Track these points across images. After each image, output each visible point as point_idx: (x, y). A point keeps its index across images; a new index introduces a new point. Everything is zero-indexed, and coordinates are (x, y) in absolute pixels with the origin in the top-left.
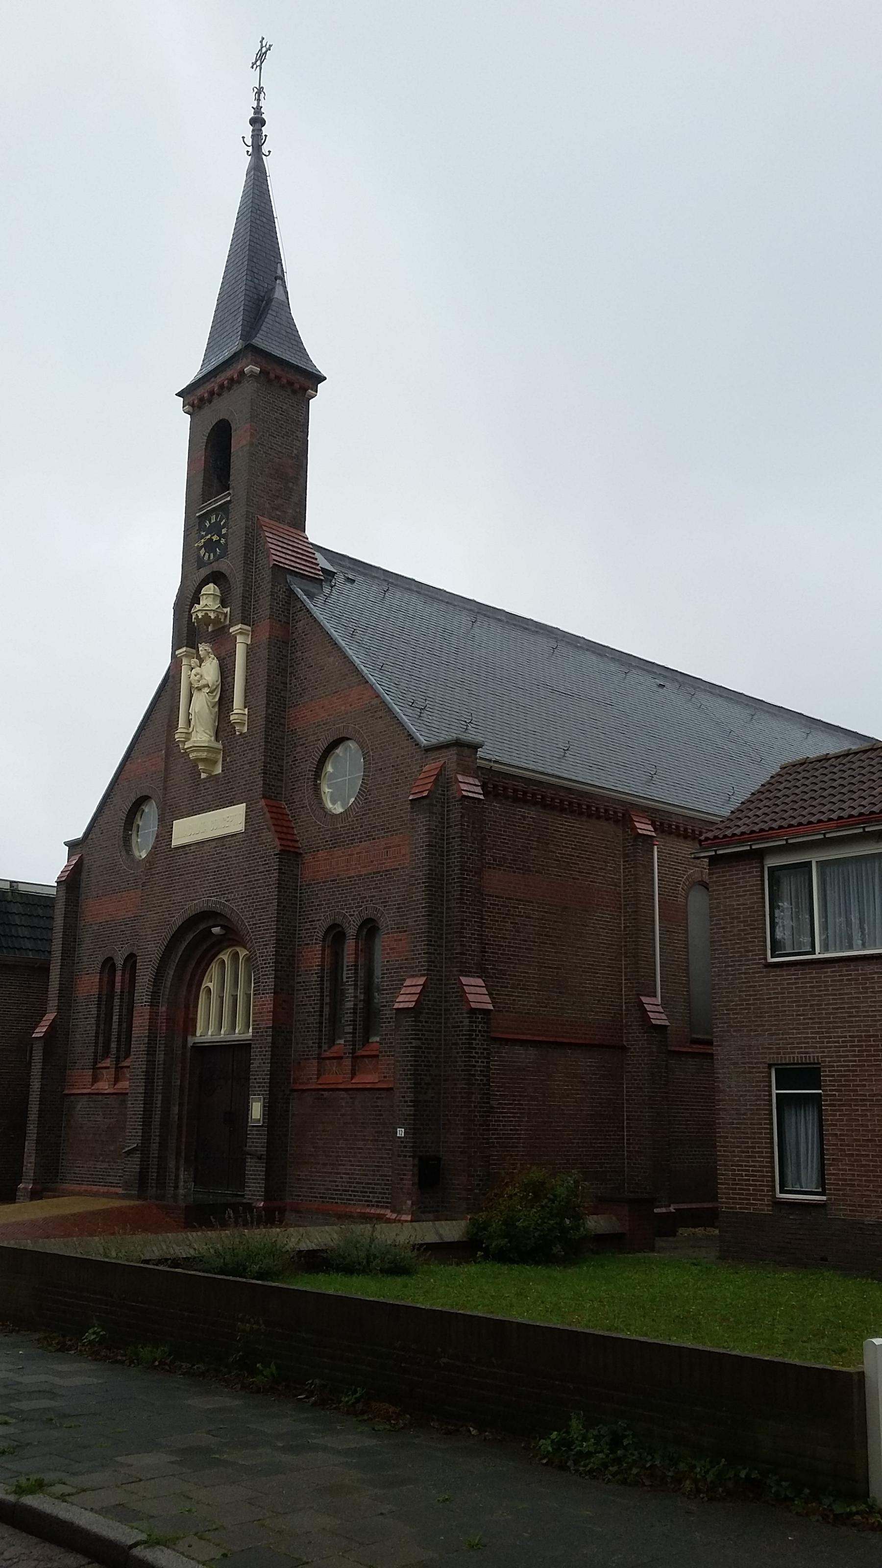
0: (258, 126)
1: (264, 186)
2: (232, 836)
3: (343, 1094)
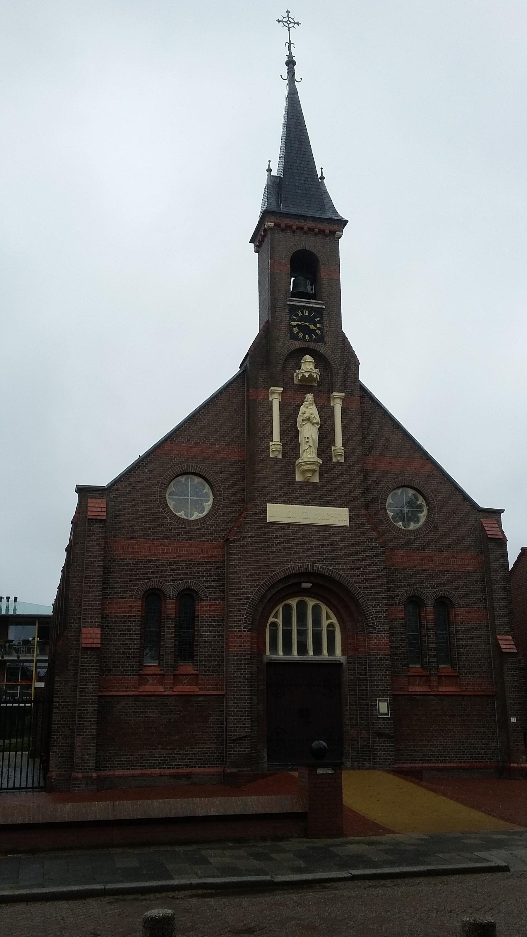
0: (291, 65)
1: (311, 157)
2: (335, 527)
3: (432, 698)
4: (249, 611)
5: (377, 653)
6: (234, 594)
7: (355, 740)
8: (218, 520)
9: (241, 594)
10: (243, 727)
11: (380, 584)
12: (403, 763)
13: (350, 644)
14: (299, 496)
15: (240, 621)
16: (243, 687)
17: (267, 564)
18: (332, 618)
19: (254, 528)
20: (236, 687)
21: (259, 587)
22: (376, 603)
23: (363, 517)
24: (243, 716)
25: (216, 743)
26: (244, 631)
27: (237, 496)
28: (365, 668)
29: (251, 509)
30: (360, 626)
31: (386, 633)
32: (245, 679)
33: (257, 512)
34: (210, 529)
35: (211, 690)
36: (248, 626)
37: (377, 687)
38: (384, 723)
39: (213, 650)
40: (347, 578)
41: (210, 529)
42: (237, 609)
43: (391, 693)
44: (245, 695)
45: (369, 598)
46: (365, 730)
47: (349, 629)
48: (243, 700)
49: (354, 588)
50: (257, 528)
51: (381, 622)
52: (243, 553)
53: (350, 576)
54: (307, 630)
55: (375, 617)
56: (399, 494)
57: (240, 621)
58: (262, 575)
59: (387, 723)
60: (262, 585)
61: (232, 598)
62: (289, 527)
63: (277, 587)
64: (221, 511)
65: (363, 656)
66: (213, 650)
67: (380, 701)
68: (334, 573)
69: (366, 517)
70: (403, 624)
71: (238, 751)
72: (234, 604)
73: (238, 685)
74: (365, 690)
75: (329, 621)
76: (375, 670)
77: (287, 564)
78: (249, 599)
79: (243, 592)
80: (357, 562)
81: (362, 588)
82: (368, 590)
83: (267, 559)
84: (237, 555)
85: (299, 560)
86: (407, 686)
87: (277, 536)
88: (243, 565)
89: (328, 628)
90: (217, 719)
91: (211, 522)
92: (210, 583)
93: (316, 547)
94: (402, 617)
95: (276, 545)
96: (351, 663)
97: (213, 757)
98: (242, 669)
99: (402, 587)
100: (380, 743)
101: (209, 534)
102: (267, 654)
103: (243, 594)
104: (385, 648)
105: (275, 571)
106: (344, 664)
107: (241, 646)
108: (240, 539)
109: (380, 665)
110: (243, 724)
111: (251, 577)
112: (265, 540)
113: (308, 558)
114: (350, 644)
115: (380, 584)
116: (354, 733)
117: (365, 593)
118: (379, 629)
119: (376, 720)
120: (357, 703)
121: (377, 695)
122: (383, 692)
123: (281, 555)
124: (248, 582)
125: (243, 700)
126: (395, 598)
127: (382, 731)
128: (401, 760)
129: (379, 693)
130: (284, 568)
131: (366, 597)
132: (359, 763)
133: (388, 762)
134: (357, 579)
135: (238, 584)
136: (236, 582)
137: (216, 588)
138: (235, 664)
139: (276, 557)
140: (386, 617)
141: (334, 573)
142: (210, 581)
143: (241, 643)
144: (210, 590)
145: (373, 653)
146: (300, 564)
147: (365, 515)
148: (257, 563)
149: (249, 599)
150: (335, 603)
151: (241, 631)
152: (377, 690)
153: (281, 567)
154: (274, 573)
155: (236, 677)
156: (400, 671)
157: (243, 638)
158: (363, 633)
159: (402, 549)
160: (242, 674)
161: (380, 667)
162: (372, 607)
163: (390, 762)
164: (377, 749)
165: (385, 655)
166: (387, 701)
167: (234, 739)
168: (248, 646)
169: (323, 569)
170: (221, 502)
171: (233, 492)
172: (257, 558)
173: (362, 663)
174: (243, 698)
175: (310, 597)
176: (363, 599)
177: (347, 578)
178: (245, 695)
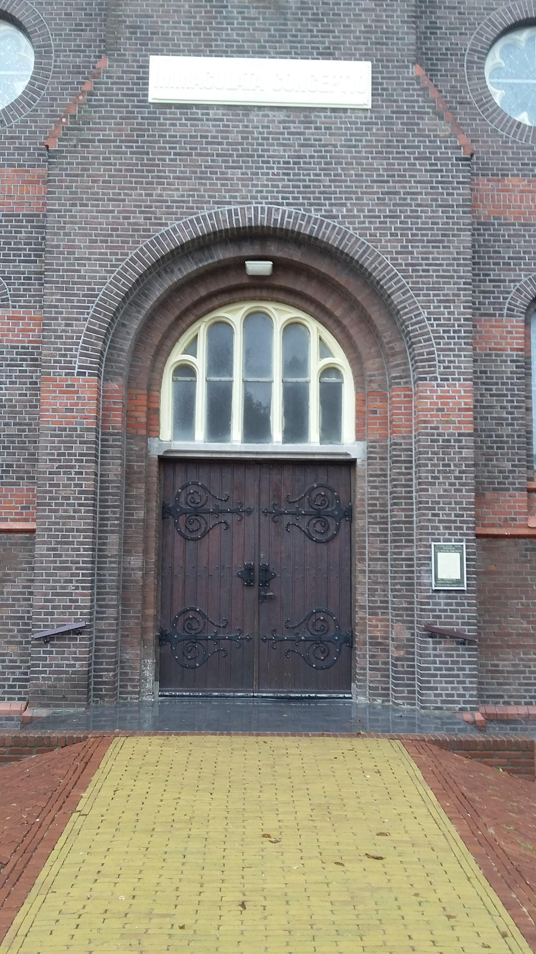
2: (334, 110)
4: (95, 325)
5: (437, 428)
6: (57, 283)
7: (380, 644)
8: (40, 116)
9: (74, 283)
10: (70, 607)
11: (451, 253)
12: (507, 703)
13: (375, 412)
14: (238, 35)
15: (71, 350)
16: (75, 511)
17: (146, 207)
18: (335, 354)
19: (115, 118)
20: (57, 511)
21: (123, 264)
22: (440, 301)
23: (412, 84)
24: (71, 581)
25: (21, 643)
26: (79, 374)
27: (90, 57)
28: (406, 468)
29: (108, 72)
30: (397, 366)
31: (465, 380)
32: (80, 492)
33: (122, 78)
34: (19, 138)
35: (12, 520)
36: (91, 362)
37: (434, 515)
38: (450, 604)
39: (20, 424)
40: (362, 239)
41: (19, 138)
42: (64, 319)
43: (473, 528)
44: (78, 530)
45: (421, 289)
46: (403, 622)
47: (370, 376)
48: (72, 543)
49: (380, 264)
50: (121, 118)
51: (453, 350)
52: (82, 181)
53: (371, 235)
54: (271, 382)
55: (435, 338)
56: (523, 45)
57: (71, 350)
58: (132, 236)
59: (457, 604)
60: (132, 259)
61: (52, 294)
62: (208, 114)
63: (180, 269)
64: (48, 94)
65: (404, 438)
66: (20, 424)
67: (439, 549)
68: (327, 228)
69: (418, 83)
70: (518, 361)
71: (57, 666)
72: (56, 307)
73: (62, 504)
74: (404, 522)
75: (327, 361)
76: (428, 471)
77: (197, 208)
78: (96, 296)
79: (79, 277)
80: (390, 200)
81: (401, 265)
82: (418, 271)
83: (146, 195)
84: (67, 187)
85: (231, 197)
86: (525, 514)
87: (175, 136)
88: (81, 211)
89: (326, 379)
90: (24, 587)
91: (22, 121)
92: (14, 267)
93: (279, 163)
94: (517, 344)
95: (171, 160)
96: (375, 458)
97: (12, 677)
98: (73, 467)
99: (520, 270)
100: (435, 656)
101: (16, 149)
102: (162, 437)
103: (80, 283)
104: (459, 416)
105: (166, 225)
106: (359, 462)
107: (72, 411)
108: (75, 146)
109: (444, 459)
110: (71, 601)
111: (102, 241)
112: (143, 147)
113: (257, 192)
114: (375, 412)
115: (451, 253)
116: (377, 626)
117: (411, 277)
118: (445, 368)
119: (429, 597)
120: (386, 553)
121: (434, 534)
122: (449, 528)
123: (185, 184)
124: (95, 253)
125: (72, 543)
126: (499, 298)
127: (441, 623)
128: (502, 697)
129: (437, 528)
130: (190, 217)
131: (412, 289)
132: (388, 701)
133: (458, 702)
134: (390, 241)
135: (69, 259)
136: (62, 253)
137: (30, 279)
138: (53, 454)
139: (171, 190)
140: (464, 338)
141: (327, 228)
142: (14, 261)
143: (71, 405)
144: (14, 284)
145: (426, 428)
146: (233, 207)
147: (418, 77)
148: (119, 206)
149: (96, 296)
150: (338, 313)
151: (73, 374)
152: (434, 521)
153: (182, 213)
154: (163, 229)
155: (58, 485)
156: (507, 478)
157: (77, 392)
158: (406, 383)
159: (524, 175)
160: (73, 479)
161: (444, 465)
162: (429, 313)
163: (465, 702)
164: (429, 669)
165: (460, 435)
166: (458, 549)
167: (45, 637)
168: (90, 411)
169: (296, 218)
170: (49, 70)
171: (80, 46)
172: (120, 194)
173: (400, 456)
174: (74, 537)
175: (278, 301)
176: (404, 294)
177: (362, 239)
178: (78, 530)
